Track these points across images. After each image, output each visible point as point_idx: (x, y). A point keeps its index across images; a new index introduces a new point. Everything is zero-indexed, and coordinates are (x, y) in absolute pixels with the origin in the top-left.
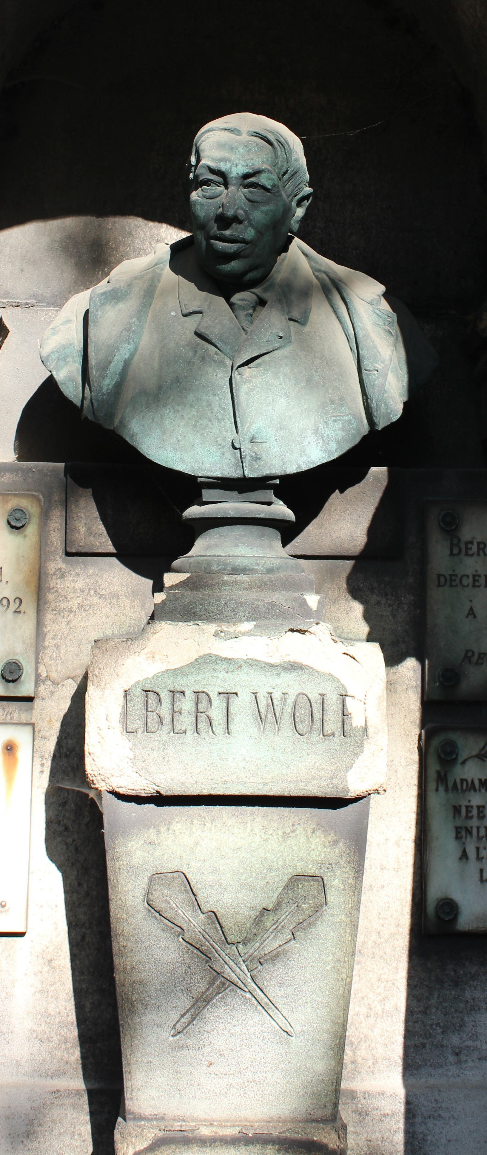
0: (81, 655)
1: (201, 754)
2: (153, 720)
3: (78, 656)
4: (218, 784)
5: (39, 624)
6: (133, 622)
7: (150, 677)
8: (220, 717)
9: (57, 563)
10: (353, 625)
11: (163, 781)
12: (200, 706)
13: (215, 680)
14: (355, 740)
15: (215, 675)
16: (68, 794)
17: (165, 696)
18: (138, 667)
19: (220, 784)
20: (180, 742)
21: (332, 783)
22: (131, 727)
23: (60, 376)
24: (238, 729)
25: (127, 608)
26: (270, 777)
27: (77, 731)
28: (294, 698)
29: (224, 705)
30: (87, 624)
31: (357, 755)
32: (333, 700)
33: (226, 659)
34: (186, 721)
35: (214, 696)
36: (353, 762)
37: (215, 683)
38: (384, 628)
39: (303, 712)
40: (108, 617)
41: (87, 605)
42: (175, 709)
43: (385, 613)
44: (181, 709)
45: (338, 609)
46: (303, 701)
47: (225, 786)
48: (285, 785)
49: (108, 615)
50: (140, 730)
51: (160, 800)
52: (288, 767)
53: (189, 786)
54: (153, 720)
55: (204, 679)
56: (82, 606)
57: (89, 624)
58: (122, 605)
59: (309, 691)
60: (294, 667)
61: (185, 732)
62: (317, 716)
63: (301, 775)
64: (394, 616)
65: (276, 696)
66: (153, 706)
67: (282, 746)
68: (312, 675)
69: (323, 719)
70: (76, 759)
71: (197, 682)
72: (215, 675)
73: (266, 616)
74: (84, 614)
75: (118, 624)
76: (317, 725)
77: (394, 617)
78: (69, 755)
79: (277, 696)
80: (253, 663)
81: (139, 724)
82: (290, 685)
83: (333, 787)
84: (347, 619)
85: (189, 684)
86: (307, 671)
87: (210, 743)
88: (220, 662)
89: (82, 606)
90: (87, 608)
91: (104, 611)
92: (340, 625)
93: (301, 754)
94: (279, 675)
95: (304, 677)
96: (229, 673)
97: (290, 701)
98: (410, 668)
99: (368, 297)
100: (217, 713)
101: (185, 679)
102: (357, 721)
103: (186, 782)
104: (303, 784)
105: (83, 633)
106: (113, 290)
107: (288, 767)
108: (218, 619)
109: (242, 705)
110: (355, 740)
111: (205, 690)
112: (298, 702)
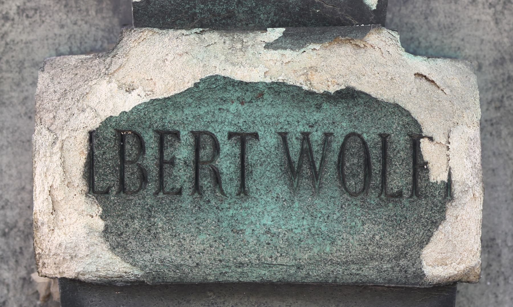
0: (23, 84)
1: (204, 224)
2: (132, 174)
3: (18, 85)
4: (229, 267)
6: (100, 34)
7: (127, 110)
8: (232, 170)
10: (434, 35)
11: (148, 264)
12: (202, 153)
13: (224, 115)
14: (433, 203)
15: (225, 107)
16: (8, 290)
17: (150, 139)
19: (233, 268)
20: (173, 206)
21: (398, 265)
22: (100, 185)
24: (259, 187)
25: (92, 12)
26: (306, 257)
27: (19, 197)
28: (342, 140)
29: (237, 151)
30: (31, 37)
31: (435, 224)
32: (400, 142)
33: (241, 82)
34: (182, 176)
35: (222, 138)
36: (429, 234)
38: (482, 41)
39: (356, 161)
40: (62, 27)
41: (32, 9)
42: (165, 158)
43: (484, 18)
44: (174, 158)
45: (412, 12)
46: (354, 146)
47: (239, 270)
48: (328, 268)
49: (64, 22)
50: (114, 190)
52: (332, 243)
53: (187, 270)
54: (132, 174)
55: (207, 113)
56: (23, 11)
57: (35, 37)
58: (83, 8)
59: (364, 130)
61: (179, 192)
62: (376, 167)
63: (353, 253)
64: (497, 22)
65: (316, 138)
67: (323, 211)
68: (369, 106)
70: (18, 239)
71: (198, 118)
72: (225, 107)
74: (27, 23)
75: (78, 36)
76: (376, 181)
77: (497, 23)
78: (9, 232)
79: (316, 136)
81: (112, 180)
83: (400, 271)
84: (425, 26)
86: (361, 101)
87: (217, 208)
88: (230, 88)
89: (23, 11)
90: (31, 13)
91: (57, 17)
92: (416, 35)
93: (354, 224)
94: (319, 107)
95: (357, 109)
96: (246, 105)
97: (336, 146)
100: (227, 165)
101: (179, 114)
102: (437, 175)
103: (181, 265)
104: (356, 267)
105: (25, 51)
106: (481, 90)
107: (332, 243)
108: (228, 24)
110: (433, 203)
111: (210, 129)
112: (348, 145)
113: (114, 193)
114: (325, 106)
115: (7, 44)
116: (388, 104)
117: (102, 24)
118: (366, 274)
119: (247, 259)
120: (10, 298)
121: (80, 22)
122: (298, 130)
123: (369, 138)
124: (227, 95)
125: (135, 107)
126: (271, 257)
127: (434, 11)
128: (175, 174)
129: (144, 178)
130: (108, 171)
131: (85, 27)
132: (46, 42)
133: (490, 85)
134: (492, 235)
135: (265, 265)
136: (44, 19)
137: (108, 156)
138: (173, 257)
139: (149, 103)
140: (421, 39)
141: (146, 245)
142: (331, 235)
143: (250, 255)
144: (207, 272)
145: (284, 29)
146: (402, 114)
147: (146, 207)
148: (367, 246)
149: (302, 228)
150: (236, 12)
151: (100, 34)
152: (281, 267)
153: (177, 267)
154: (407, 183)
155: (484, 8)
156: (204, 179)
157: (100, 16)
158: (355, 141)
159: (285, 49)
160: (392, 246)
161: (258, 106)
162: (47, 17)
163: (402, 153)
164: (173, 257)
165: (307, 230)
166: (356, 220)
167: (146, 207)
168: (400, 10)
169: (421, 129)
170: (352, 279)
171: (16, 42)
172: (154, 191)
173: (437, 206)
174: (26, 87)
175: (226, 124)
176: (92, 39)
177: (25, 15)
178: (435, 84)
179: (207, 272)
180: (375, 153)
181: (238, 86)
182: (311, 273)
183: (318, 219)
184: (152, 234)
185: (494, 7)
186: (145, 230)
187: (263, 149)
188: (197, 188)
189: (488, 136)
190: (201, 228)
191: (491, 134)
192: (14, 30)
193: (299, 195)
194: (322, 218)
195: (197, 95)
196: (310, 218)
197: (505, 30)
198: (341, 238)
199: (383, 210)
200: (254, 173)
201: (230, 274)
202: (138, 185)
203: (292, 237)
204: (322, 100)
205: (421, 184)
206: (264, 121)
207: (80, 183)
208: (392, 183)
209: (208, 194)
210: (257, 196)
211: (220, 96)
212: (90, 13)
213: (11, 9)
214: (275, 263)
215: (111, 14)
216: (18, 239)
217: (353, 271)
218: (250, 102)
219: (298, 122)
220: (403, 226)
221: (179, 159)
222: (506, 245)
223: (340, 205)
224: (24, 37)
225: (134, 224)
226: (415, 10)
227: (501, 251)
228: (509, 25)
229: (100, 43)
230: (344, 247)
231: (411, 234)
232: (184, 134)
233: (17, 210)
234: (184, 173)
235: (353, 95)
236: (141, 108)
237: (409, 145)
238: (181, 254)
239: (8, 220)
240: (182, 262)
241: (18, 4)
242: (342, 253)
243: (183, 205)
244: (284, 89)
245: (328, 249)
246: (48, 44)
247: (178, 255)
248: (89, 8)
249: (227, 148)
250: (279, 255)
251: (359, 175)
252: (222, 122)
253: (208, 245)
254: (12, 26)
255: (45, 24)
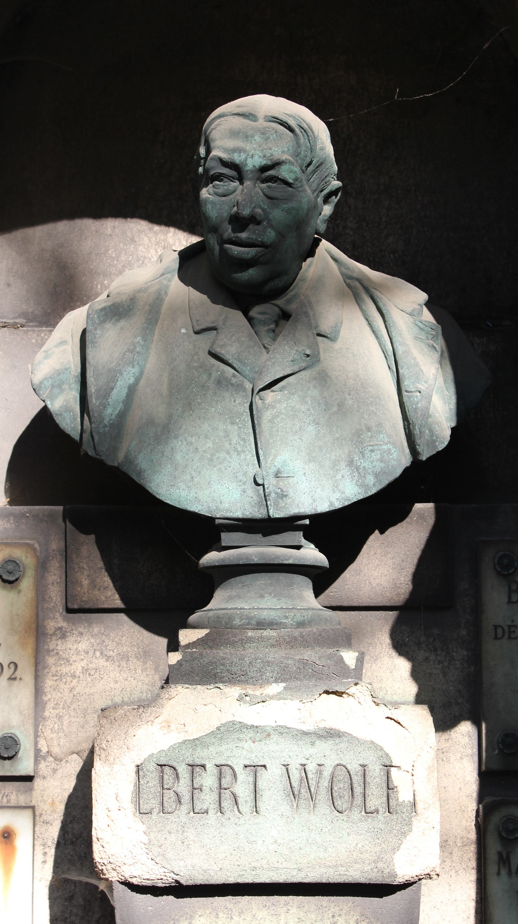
0: (87, 726)
2: (169, 798)
3: (83, 727)
4: (246, 871)
5: (38, 692)
6: (145, 687)
8: (246, 794)
9: (57, 621)
12: (223, 781)
13: (240, 751)
15: (240, 745)
16: (75, 886)
17: (183, 770)
18: (151, 738)
23: (55, 406)
25: (139, 671)
26: (305, 861)
28: (331, 770)
29: (251, 779)
30: (92, 691)
31: (404, 834)
32: (375, 771)
34: (207, 799)
36: (400, 842)
37: (239, 754)
39: (342, 786)
40: (116, 682)
41: (93, 669)
42: (196, 786)
44: (202, 785)
46: (341, 773)
47: (253, 873)
51: (180, 890)
53: (212, 874)
54: (169, 798)
55: (227, 750)
58: (132, 668)
60: (331, 734)
61: (207, 812)
62: (358, 790)
63: (341, 858)
66: (170, 783)
67: (318, 825)
69: (363, 790)
73: (299, 678)
74: (89, 679)
76: (359, 800)
79: (311, 768)
80: (283, 731)
81: (154, 803)
82: (327, 755)
83: (378, 871)
85: (210, 756)
86: (345, 739)
87: (236, 824)
88: (245, 730)
90: (92, 672)
93: (341, 835)
94: (313, 744)
95: (342, 745)
96: (256, 743)
97: (327, 773)
98: (465, 731)
99: (408, 304)
100: (243, 788)
101: (205, 751)
102: (404, 795)
104: (343, 869)
109: (272, 780)
111: (229, 763)
113: (156, 813)
114: (318, 743)
115: (74, 696)
116: (365, 742)
117: (146, 680)
118: (352, 874)
119: (259, 864)
120: (77, 893)
121: (129, 679)
122: (298, 762)
123: (352, 768)
124: (241, 736)
125: (171, 746)
126: (278, 862)
127: (396, 667)
128: (202, 797)
129: (179, 801)
130: (151, 796)
131: (134, 682)
132: (104, 694)
133: (441, 723)
134: (445, 838)
135: (273, 869)
136: (102, 676)
137: (150, 784)
138: (202, 864)
139: (182, 743)
140: (387, 688)
141: (180, 854)
142: (324, 844)
143: (261, 861)
144: (228, 875)
145: (284, 685)
146: (376, 748)
147: (181, 824)
148: (352, 852)
149: (302, 839)
150: (248, 671)
151: (145, 687)
152: (285, 870)
153: (205, 871)
154: (382, 803)
155: (435, 664)
156: (225, 801)
157: (144, 673)
158: (341, 770)
159: (287, 699)
160: (371, 852)
161: (266, 743)
162: (105, 675)
163: (377, 779)
164: (202, 864)
165: (305, 840)
166: (344, 832)
167: (181, 824)
168: (371, 666)
169: (391, 761)
170: (341, 878)
171: (81, 694)
172: (186, 812)
173: (405, 821)
174: (89, 729)
175: (242, 758)
176: (139, 691)
177: (88, 673)
178: (401, 725)
179: (228, 875)
180: (357, 780)
181: (250, 729)
182: (309, 874)
183: (314, 831)
184: (186, 846)
185: (442, 663)
186: (180, 843)
187: (270, 778)
188: (221, 810)
189: (440, 761)
190: (223, 840)
191: (442, 760)
192: (80, 685)
193: (299, 813)
194: (317, 831)
195: (219, 736)
196: (308, 831)
197: (451, 681)
198: (331, 846)
199: (363, 823)
200: (264, 796)
201: (246, 876)
202: (174, 807)
203: (294, 846)
204: (315, 738)
205: (392, 803)
206: (270, 756)
207: (129, 807)
208: (370, 803)
209: (228, 814)
210: (266, 814)
211: (237, 737)
212: (137, 671)
213: (77, 670)
214: (280, 867)
215: (153, 672)
216: (83, 846)
217: (342, 872)
218: (260, 741)
219: (297, 756)
220: (380, 836)
221: (206, 786)
222: (456, 845)
223: (331, 821)
224: (87, 690)
225: (171, 838)
226: (382, 666)
227: (452, 850)
228: (454, 676)
229: (145, 694)
230: (334, 853)
231: (386, 842)
232: (209, 766)
233: (82, 824)
234: (210, 797)
235: (339, 734)
236: (176, 747)
237: (383, 773)
238: (208, 861)
239: (75, 832)
240: (209, 868)
241: (83, 666)
242: (333, 859)
243: (209, 822)
244: (286, 730)
245: (322, 856)
246: (106, 695)
247: (206, 862)
248: (137, 667)
249: (243, 777)
250: (284, 860)
251: (344, 797)
252: (238, 757)
253: (229, 854)
254: (78, 682)
255: (103, 680)
